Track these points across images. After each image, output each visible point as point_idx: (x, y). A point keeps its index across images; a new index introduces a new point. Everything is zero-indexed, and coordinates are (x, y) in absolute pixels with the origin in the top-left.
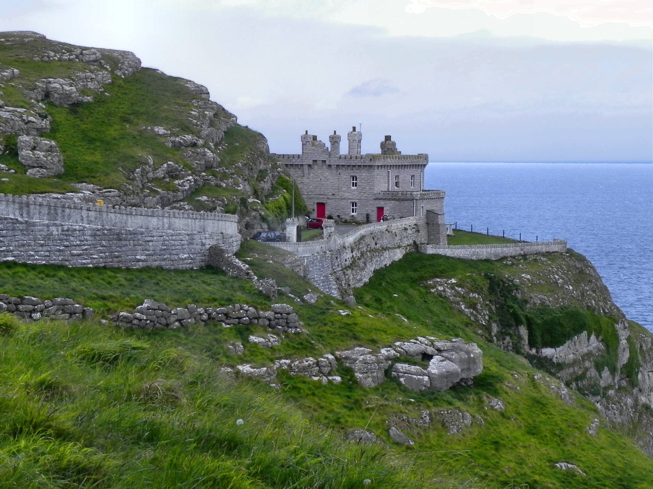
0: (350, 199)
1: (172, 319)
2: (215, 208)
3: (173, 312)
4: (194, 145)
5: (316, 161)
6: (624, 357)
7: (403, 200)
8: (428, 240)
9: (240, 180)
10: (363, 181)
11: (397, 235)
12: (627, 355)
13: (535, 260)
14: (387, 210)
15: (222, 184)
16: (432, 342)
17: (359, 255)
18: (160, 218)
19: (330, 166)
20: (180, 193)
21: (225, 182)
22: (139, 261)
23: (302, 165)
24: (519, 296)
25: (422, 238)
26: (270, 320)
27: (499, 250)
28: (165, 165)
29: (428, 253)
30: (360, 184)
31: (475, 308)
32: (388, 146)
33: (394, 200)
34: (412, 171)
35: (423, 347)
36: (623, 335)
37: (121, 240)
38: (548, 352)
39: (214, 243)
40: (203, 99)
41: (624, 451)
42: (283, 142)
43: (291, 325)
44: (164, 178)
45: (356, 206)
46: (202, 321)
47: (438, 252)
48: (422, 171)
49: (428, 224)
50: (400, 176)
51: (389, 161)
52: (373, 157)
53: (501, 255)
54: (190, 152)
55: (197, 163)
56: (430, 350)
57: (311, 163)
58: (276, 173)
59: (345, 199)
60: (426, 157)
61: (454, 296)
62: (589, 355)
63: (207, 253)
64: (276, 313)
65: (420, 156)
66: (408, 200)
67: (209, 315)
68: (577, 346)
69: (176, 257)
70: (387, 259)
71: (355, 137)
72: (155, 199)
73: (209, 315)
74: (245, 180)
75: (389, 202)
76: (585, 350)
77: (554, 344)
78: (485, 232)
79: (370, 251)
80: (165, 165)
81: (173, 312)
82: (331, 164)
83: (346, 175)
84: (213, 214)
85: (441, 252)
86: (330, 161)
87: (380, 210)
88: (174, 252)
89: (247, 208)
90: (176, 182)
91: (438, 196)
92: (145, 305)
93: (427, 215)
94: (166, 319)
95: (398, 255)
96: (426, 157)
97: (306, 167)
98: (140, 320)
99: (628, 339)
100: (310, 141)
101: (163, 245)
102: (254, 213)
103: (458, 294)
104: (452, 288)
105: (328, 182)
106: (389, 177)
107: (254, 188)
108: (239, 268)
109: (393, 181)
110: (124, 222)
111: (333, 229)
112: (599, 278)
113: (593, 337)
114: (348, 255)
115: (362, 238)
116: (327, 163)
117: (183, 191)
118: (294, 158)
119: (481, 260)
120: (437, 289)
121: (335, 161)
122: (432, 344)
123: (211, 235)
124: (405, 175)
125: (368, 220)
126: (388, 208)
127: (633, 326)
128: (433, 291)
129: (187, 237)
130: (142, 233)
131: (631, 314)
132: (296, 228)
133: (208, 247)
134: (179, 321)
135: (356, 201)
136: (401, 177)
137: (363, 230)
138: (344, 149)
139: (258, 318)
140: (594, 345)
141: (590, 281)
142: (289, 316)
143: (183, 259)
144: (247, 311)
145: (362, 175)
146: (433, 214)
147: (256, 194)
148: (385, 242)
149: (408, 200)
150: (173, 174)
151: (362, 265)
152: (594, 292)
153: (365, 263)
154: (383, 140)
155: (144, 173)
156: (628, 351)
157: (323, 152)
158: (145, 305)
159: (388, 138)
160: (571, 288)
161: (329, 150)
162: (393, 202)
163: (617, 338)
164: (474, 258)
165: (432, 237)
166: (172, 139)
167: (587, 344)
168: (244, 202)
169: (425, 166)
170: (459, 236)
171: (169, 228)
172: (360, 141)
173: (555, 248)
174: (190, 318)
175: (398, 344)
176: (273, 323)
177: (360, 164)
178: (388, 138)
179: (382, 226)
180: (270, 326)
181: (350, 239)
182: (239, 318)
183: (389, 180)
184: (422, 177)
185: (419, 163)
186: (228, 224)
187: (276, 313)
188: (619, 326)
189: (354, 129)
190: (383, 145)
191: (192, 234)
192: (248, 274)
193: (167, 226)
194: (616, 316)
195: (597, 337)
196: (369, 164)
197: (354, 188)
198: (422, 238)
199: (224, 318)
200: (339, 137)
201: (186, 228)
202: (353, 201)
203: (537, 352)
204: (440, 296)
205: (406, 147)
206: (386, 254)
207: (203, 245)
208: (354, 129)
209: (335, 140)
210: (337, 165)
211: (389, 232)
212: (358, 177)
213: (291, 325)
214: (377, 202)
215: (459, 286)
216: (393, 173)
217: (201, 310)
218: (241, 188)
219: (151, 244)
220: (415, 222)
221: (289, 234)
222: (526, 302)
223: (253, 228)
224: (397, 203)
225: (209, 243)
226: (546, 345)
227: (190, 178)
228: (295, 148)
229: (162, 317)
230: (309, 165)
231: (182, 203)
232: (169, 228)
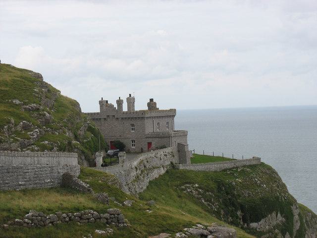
1: (48, 222)
2: (53, 148)
3: (48, 217)
4: (38, 109)
6: (297, 226)
7: (163, 137)
9: (66, 130)
11: (160, 160)
12: (299, 224)
13: (243, 170)
16: (206, 227)
17: (140, 173)
18: (32, 158)
19: (117, 119)
20: (32, 140)
22: (21, 185)
24: (235, 192)
25: (175, 160)
26: (107, 219)
27: (222, 165)
28: (21, 123)
31: (210, 201)
32: (152, 104)
34: (166, 120)
35: (201, 231)
36: (296, 212)
37: (9, 173)
38: (254, 225)
39: (66, 171)
40: (40, 82)
41: (62, 202)
42: (89, 106)
43: (120, 221)
44: (21, 131)
46: (66, 222)
48: (173, 119)
49: (179, 151)
51: (153, 114)
52: (143, 112)
53: (223, 168)
54: (35, 114)
55: (40, 121)
56: (205, 232)
59: (127, 138)
62: (277, 226)
63: (61, 178)
64: (111, 215)
65: (171, 110)
66: (167, 137)
67: (70, 218)
68: (271, 221)
69: (43, 181)
70: (155, 174)
71: (131, 101)
72: (17, 144)
73: (70, 218)
75: (154, 139)
76: (275, 223)
77: (257, 220)
79: (146, 170)
80: (21, 123)
81: (48, 217)
83: (127, 124)
84: (64, 153)
85: (188, 168)
87: (150, 144)
88: (42, 178)
90: (29, 133)
91: (184, 134)
92: (30, 214)
93: (178, 146)
94: (43, 222)
95: (163, 171)
98: (28, 223)
99: (299, 215)
100: (103, 104)
101: (35, 174)
103: (199, 193)
104: (196, 190)
107: (74, 134)
108: (83, 187)
109: (156, 126)
110: (10, 161)
111: (125, 157)
112: (280, 179)
113: (279, 215)
114: (134, 173)
115: (142, 161)
117: (33, 139)
121: (121, 115)
122: (206, 228)
123: (63, 167)
124: (163, 122)
125: (142, 151)
127: (302, 208)
129: (49, 169)
130: (22, 168)
131: (301, 200)
132: (102, 158)
133: (62, 174)
134: (52, 223)
136: (161, 123)
137: (142, 157)
138: (125, 108)
139: (100, 218)
140: (280, 219)
141: (276, 182)
142: (119, 216)
143: (47, 183)
144: (93, 214)
145: (138, 123)
147: (76, 138)
148: (154, 164)
149: (167, 137)
150: (26, 128)
151: (142, 178)
152: (278, 187)
153: (143, 177)
155: (9, 128)
156: (299, 221)
158: (30, 214)
159: (151, 100)
160: (265, 186)
163: (292, 215)
166: (25, 106)
167: (276, 219)
168: (70, 143)
169: (174, 116)
171: (38, 164)
172: (134, 103)
173: (254, 163)
174: (58, 220)
175: (186, 229)
176: (110, 221)
178: (151, 100)
179: (152, 154)
180: (107, 223)
181: (135, 163)
182: (88, 219)
184: (173, 122)
186: (73, 159)
187: (111, 215)
188: (293, 208)
189: (130, 95)
190: (149, 105)
191: (52, 167)
192: (89, 190)
193: (36, 162)
194: (291, 201)
195: (281, 215)
196: (141, 116)
197: (133, 131)
198: (175, 160)
199: (79, 219)
200: (122, 101)
201: (48, 163)
203: (247, 225)
205: (161, 106)
206: (156, 171)
207: (59, 173)
208: (130, 95)
209: (120, 102)
210: (122, 118)
213: (120, 221)
214: (147, 139)
215: (200, 188)
216: (156, 121)
217: (64, 215)
219: (27, 174)
220: (171, 151)
222: (239, 196)
225: (62, 172)
226: (252, 221)
227: (37, 130)
228: (96, 109)
229: (41, 221)
230: (105, 119)
231: (33, 146)
232: (38, 164)
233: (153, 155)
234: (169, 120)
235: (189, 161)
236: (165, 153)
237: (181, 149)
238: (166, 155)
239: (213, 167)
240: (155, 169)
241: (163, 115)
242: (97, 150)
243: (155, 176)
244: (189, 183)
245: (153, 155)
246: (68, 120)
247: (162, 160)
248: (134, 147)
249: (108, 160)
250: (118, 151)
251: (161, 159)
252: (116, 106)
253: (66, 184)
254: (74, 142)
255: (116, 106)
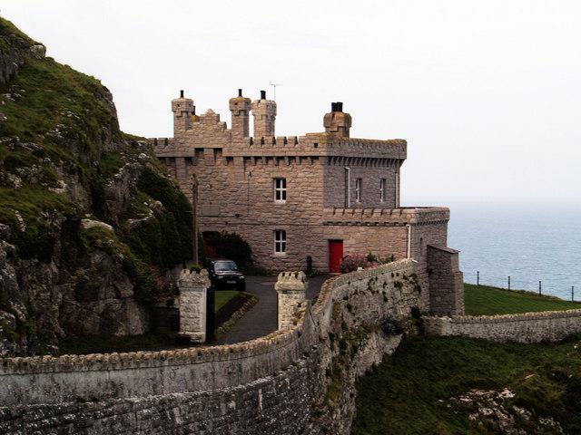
0: (270, 224)
5: (202, 149)
8: (431, 306)
10: (300, 189)
14: (351, 246)
15: (12, 178)
19: (230, 159)
21: (18, 174)
23: (173, 159)
29: (444, 333)
30: (291, 194)
33: (365, 224)
45: (284, 238)
47: (462, 330)
48: (397, 172)
49: (429, 272)
50: (364, 180)
57: (191, 153)
58: (137, 164)
59: (261, 223)
60: (401, 146)
61: (514, 427)
65: (391, 144)
74: (72, 172)
75: (353, 229)
78: (535, 289)
82: (234, 154)
86: (230, 151)
89: (80, 244)
96: (401, 146)
97: (180, 163)
102: (97, 258)
105: (227, 191)
106: (346, 181)
116: (225, 153)
118: (156, 144)
119: (536, 343)
120: (481, 414)
126: (352, 241)
128: (472, 417)
135: (285, 228)
146: (439, 253)
154: (329, 110)
157: (217, 131)
159: (337, 107)
161: (229, 127)
162: (362, 229)
164: (522, 339)
165: (438, 299)
168: (72, 225)
170: (488, 299)
177: (293, 154)
178: (337, 107)
183: (346, 186)
185: (390, 156)
189: (263, 93)
190: (328, 120)
197: (281, 201)
202: (278, 227)
204: (490, 428)
208: (263, 93)
210: (246, 158)
211: (373, 293)
212: (288, 180)
214: (329, 229)
215: (520, 403)
218: (62, 188)
221: (187, 309)
223: (95, 298)
224: (372, 231)
233: (363, 285)
234: (382, 172)
235: (460, 306)
236: (396, 279)
237: (438, 262)
238: (398, 285)
239: (540, 326)
240: (370, 332)
241: (374, 156)
242: (183, 259)
243: (371, 360)
244: (482, 386)
245: (363, 285)
246: (70, 135)
247: (390, 302)
248: (281, 254)
249: (223, 298)
250: (425, 314)
251: (386, 300)
252: (227, 117)
253: (67, 368)
254: (89, 223)
255: (227, 117)
